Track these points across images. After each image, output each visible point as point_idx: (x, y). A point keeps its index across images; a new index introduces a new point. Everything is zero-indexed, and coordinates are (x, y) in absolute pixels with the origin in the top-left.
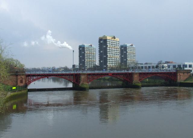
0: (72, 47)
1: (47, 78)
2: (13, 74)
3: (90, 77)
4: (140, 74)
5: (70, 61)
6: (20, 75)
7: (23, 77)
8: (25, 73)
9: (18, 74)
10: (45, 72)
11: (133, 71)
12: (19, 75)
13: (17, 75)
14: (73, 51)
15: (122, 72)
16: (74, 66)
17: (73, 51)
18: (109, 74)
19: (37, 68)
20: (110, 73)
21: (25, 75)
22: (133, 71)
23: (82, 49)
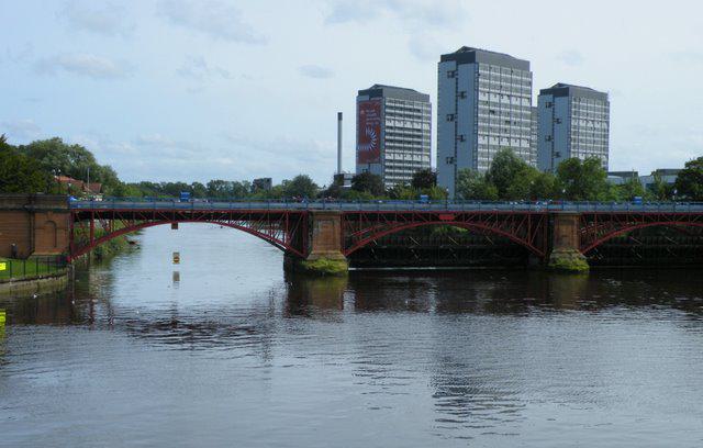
0: (304, 266)
1: (170, 225)
2: (565, 218)
3: (149, 192)
4: (586, 218)
5: (322, 151)
6: (45, 211)
7: (59, 219)
8: (67, 201)
9: (35, 207)
10: (158, 203)
11: (551, 207)
12: (39, 211)
13: (31, 213)
14: (340, 115)
15: (532, 206)
16: (339, 178)
17: (340, 115)
18: (441, 217)
19: (101, 160)
20: (448, 213)
21: (65, 212)
22: (551, 207)
23: (373, 103)
